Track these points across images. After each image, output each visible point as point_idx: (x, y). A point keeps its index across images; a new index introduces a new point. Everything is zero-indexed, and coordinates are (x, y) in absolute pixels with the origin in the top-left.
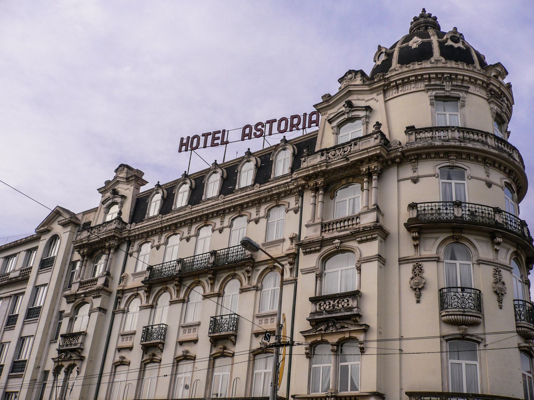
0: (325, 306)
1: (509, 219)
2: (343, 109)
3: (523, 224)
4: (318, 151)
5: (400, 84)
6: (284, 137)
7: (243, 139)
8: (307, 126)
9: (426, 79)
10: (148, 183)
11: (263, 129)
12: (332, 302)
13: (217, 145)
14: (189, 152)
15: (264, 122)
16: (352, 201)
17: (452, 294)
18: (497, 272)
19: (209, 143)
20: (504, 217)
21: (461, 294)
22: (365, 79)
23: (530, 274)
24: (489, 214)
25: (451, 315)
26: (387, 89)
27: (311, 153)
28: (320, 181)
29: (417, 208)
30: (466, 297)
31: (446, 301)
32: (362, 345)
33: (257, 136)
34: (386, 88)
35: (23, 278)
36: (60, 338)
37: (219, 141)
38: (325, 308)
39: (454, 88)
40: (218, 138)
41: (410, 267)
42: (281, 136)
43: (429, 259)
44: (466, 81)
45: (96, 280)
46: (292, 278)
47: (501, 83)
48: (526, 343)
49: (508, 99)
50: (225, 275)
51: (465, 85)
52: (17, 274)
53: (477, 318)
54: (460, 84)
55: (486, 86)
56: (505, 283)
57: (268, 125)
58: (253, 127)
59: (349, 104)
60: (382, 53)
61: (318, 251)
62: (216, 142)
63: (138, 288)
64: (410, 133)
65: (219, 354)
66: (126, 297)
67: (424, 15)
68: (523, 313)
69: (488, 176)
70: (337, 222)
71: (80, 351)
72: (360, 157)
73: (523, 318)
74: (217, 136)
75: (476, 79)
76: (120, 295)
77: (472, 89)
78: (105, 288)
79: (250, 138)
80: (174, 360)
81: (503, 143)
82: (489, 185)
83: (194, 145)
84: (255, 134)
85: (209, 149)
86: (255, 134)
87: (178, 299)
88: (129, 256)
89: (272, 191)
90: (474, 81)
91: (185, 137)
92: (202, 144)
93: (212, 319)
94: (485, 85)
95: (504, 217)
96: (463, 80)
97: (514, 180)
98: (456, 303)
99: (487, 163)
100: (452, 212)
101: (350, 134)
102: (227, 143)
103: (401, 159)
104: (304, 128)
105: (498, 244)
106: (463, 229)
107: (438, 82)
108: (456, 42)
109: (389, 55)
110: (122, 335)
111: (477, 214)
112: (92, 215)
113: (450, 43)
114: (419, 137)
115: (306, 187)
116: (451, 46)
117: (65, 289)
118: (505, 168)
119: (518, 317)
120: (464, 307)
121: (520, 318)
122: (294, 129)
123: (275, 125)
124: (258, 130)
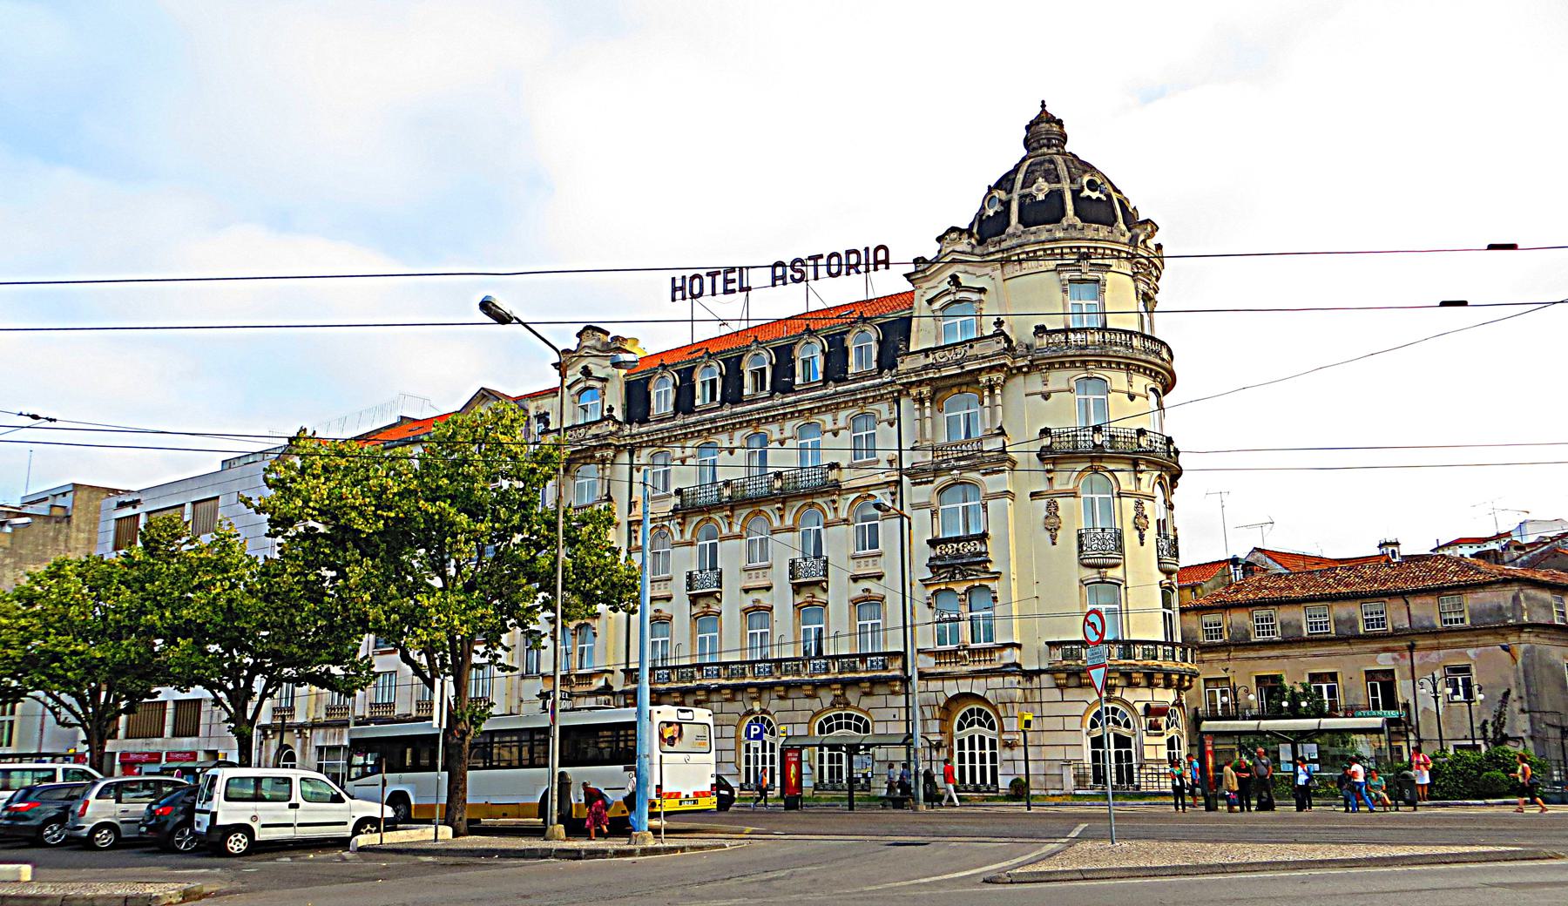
5: (1023, 260)
7: (774, 285)
12: (955, 545)
13: (733, 291)
14: (688, 301)
18: (1139, 505)
19: (720, 288)
28: (925, 390)
32: (835, 471)
33: (794, 280)
37: (735, 286)
40: (733, 281)
41: (1044, 502)
43: (1065, 494)
50: (799, 504)
61: (932, 482)
62: (730, 287)
74: (730, 276)
75: (1119, 251)
79: (785, 284)
85: (720, 297)
86: (792, 276)
102: (749, 289)
113: (1087, 192)
114: (1051, 341)
118: (1151, 372)
122: (852, 271)
124: (797, 271)
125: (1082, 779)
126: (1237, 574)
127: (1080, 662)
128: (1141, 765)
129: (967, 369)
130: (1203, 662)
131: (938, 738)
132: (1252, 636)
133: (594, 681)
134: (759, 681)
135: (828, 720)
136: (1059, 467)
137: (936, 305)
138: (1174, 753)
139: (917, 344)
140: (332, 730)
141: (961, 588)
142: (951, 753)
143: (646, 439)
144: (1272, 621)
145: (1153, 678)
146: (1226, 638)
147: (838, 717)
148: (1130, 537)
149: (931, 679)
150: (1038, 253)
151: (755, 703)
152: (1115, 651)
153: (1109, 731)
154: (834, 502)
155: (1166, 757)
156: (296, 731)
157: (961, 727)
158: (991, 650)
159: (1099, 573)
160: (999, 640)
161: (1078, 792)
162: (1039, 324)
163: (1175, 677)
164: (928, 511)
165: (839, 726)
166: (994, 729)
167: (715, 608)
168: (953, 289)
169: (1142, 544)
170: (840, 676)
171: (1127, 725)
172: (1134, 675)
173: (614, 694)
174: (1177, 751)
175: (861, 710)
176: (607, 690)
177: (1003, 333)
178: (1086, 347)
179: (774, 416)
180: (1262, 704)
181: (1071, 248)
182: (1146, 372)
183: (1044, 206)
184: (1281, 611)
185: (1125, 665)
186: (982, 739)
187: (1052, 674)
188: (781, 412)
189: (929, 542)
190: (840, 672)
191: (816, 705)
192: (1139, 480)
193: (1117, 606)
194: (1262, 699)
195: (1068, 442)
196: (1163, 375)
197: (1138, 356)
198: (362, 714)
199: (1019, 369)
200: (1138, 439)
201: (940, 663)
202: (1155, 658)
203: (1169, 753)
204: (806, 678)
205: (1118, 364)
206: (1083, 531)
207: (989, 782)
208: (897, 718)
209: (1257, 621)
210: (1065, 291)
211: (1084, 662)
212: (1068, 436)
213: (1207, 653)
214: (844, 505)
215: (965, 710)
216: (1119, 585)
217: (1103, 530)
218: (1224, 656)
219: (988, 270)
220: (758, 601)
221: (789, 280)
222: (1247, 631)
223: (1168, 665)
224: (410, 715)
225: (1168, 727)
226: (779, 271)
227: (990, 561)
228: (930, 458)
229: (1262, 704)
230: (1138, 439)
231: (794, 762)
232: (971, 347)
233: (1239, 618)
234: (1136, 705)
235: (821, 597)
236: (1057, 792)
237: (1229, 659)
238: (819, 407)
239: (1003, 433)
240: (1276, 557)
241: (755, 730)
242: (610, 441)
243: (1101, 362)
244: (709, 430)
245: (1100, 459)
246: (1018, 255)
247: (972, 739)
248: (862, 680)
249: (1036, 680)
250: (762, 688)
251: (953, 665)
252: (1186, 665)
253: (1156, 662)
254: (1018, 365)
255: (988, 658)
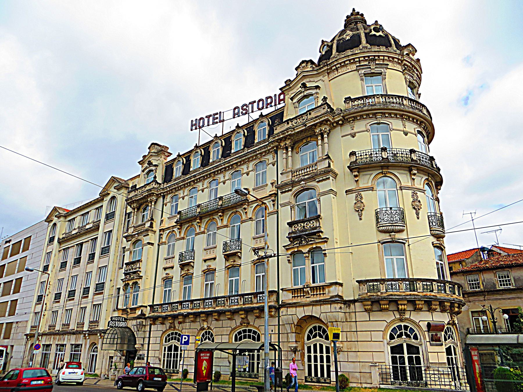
0: (298, 228)
1: (421, 156)
2: (300, 89)
3: (432, 159)
4: (285, 121)
5: (339, 67)
6: (261, 113)
7: (234, 117)
8: (277, 103)
9: (357, 61)
10: (172, 154)
11: (247, 108)
12: (302, 224)
13: (217, 123)
15: (248, 103)
16: (311, 154)
17: (384, 212)
18: (414, 194)
19: (211, 123)
20: (418, 155)
21: (390, 211)
22: (314, 66)
23: (438, 193)
24: (406, 154)
25: (384, 226)
26: (330, 72)
27: (281, 122)
29: (355, 155)
30: (394, 213)
31: (380, 217)
34: (329, 71)
35: (96, 228)
36: (125, 266)
38: (298, 229)
39: (377, 66)
40: (217, 118)
42: (259, 113)
44: (386, 60)
45: (145, 224)
46: (275, 211)
47: (412, 59)
48: (438, 241)
49: (417, 70)
51: (385, 63)
52: (91, 225)
53: (402, 227)
54: (382, 63)
55: (400, 62)
56: (421, 201)
57: (250, 106)
58: (240, 108)
59: (304, 85)
60: (325, 45)
61: (291, 190)
62: (216, 121)
63: (173, 226)
64: (347, 102)
65: (231, 266)
66: (165, 233)
67: (354, 13)
68: (434, 220)
69: (405, 127)
70: (302, 170)
71: (139, 272)
72: (314, 123)
73: (434, 224)
74: (216, 116)
75: (393, 58)
76: (162, 233)
77: (391, 65)
78: (151, 229)
79: (239, 116)
80: (180, 278)
81: (415, 103)
82: (406, 134)
83: (201, 125)
84: (242, 112)
87: (180, 237)
88: (164, 205)
89: (256, 152)
90: (392, 59)
91: (194, 120)
92: (206, 124)
93: (224, 243)
94: (400, 61)
95: (418, 155)
96: (383, 60)
97: (424, 129)
98: (387, 218)
99: (404, 118)
100: (381, 155)
101: (306, 107)
102: (223, 121)
103: (343, 122)
104: (275, 105)
105: (414, 174)
106: (389, 166)
107: (367, 63)
108: (378, 32)
109: (331, 47)
110: (205, 250)
111: (398, 155)
112: (137, 179)
113: (373, 33)
114: (354, 104)
115: (279, 147)
116: (375, 35)
117: (123, 233)
118: (417, 121)
119: (431, 224)
120: (392, 220)
121: (432, 224)
122: (269, 106)
123: (255, 105)
125: (384, 376)
126: (485, 256)
127: (379, 293)
128: (428, 367)
129: (308, 125)
130: (470, 302)
131: (294, 345)
132: (497, 286)
133: (137, 311)
134: (205, 310)
135: (240, 333)
136: (362, 174)
137: (295, 100)
138: (452, 358)
139: (434, 276)
140: (48, 337)
141: (305, 250)
142: (303, 355)
143: (168, 189)
144: (508, 277)
145: (431, 305)
146: (482, 288)
147: (245, 331)
148: (410, 214)
149: (290, 307)
150: (346, 63)
151: (204, 323)
152: (403, 286)
153: (404, 341)
154: (245, 209)
155: (446, 361)
156: (98, 335)
157: (309, 338)
158: (323, 287)
159: (390, 236)
160: (328, 281)
161: (382, 386)
162: (347, 97)
163: (448, 304)
164: (289, 206)
165: (245, 337)
166: (328, 340)
167: (191, 271)
168: (303, 90)
169: (418, 218)
170: (243, 307)
171: (416, 337)
172: (417, 302)
173: (145, 319)
174: (453, 356)
175: (255, 327)
176: (143, 314)
177: (327, 103)
178: (375, 105)
179: (220, 170)
180: (508, 326)
181: (364, 57)
182: (414, 120)
183: (349, 42)
184: (513, 271)
185: (410, 295)
186: (321, 346)
187: (362, 302)
188: (223, 167)
189: (288, 224)
190: (244, 304)
191: (233, 324)
192: (414, 179)
193: (404, 257)
194: (507, 323)
195: (366, 158)
196: (425, 124)
197: (407, 109)
198: (59, 329)
199: (337, 122)
200: (411, 155)
201: (295, 297)
202: (432, 291)
203: (448, 358)
204: (227, 308)
205: (396, 115)
206: (378, 210)
207: (326, 376)
208: (273, 332)
209: (499, 278)
210: (362, 80)
211: (382, 293)
212: (366, 155)
213: (471, 296)
214: (250, 211)
215: (311, 327)
216: (404, 243)
217: (391, 208)
218: (482, 298)
219: (321, 77)
220: (210, 266)
221: (241, 114)
222: (493, 283)
223: (442, 296)
224: (74, 329)
225: (445, 340)
226: (236, 111)
227: (322, 232)
228: (290, 177)
229: (508, 326)
230: (411, 155)
231: (206, 360)
232: (310, 114)
233: (488, 277)
234: (421, 323)
235: (238, 262)
236: (369, 386)
237: (485, 300)
238: (240, 162)
239: (329, 157)
240: (504, 250)
241: (185, 338)
242: (153, 192)
243: (384, 113)
244: (193, 181)
245: (387, 167)
246: (335, 65)
247: (315, 346)
248: (253, 309)
249: (352, 306)
250: (209, 314)
251: (302, 297)
252: (455, 296)
253: (433, 294)
254: (336, 120)
255: (322, 292)
